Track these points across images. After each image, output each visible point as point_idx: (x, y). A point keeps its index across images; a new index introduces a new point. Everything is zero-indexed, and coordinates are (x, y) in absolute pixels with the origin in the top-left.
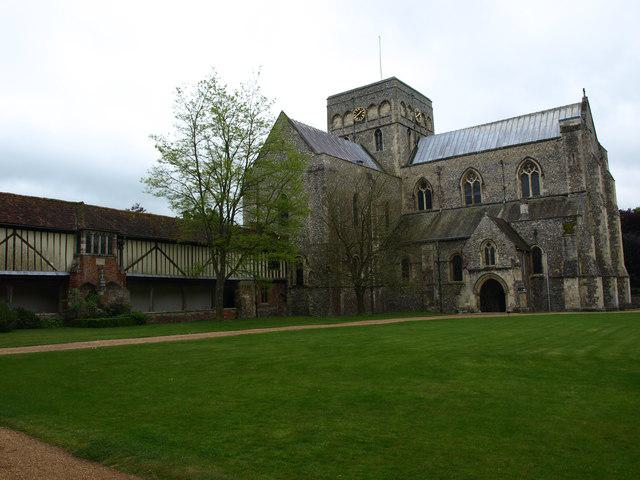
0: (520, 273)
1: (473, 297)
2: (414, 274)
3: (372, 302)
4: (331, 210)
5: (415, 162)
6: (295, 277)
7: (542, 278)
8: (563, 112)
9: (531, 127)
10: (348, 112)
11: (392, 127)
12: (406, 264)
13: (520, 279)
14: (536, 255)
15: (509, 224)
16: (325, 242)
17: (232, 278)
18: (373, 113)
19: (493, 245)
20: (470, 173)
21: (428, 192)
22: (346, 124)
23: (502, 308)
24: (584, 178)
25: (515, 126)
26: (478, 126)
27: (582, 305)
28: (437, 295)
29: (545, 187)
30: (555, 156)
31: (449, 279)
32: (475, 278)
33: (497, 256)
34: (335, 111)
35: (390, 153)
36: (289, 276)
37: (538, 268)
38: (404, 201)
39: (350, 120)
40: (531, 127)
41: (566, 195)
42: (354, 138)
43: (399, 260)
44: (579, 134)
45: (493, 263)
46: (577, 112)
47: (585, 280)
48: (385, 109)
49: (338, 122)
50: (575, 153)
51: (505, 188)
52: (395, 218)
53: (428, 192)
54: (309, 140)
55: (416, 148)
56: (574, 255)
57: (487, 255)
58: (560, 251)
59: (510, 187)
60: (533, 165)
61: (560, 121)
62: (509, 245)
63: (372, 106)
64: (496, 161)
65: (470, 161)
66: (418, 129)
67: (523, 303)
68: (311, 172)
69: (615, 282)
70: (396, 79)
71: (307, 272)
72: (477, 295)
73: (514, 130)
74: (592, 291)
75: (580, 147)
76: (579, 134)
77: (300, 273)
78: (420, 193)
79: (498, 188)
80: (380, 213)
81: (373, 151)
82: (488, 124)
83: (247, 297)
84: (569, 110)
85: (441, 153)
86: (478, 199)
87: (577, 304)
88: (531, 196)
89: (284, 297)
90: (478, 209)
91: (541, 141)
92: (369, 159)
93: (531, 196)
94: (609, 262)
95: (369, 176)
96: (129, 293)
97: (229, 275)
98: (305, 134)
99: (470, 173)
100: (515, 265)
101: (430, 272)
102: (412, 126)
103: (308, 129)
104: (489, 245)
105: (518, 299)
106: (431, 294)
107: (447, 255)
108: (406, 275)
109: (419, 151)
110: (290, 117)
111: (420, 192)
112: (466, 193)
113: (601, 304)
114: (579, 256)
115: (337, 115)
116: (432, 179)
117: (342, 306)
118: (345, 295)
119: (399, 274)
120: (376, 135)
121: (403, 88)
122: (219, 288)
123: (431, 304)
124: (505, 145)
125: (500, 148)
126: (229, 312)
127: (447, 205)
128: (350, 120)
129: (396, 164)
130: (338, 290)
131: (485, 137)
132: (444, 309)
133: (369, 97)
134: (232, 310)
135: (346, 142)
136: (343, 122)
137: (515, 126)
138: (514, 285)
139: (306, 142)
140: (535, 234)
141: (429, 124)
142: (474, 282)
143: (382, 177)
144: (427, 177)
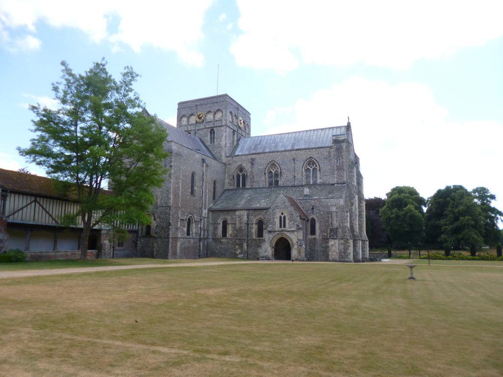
10: (192, 115)
11: (222, 128)
17: (96, 227)
18: (210, 117)
20: (273, 164)
21: (244, 175)
23: (288, 257)
24: (345, 174)
29: (320, 178)
32: (271, 236)
34: (183, 113)
35: (219, 146)
36: (140, 228)
37: (313, 232)
39: (193, 120)
43: (220, 221)
44: (344, 145)
45: (284, 227)
46: (343, 131)
47: (342, 241)
48: (219, 115)
51: (295, 177)
53: (244, 175)
55: (238, 144)
56: (336, 224)
58: (328, 221)
59: (298, 176)
60: (314, 163)
61: (333, 136)
63: (209, 112)
66: (240, 131)
72: (273, 248)
75: (344, 154)
76: (344, 145)
78: (238, 176)
81: (208, 144)
86: (277, 182)
94: (357, 230)
97: (94, 225)
99: (273, 164)
100: (299, 229)
102: (236, 129)
109: (240, 146)
113: (351, 257)
115: (184, 116)
116: (247, 166)
117: (178, 251)
118: (181, 244)
120: (211, 133)
121: (232, 102)
122: (86, 235)
125: (294, 150)
126: (92, 253)
128: (193, 120)
132: (249, 256)
134: (94, 252)
136: (188, 121)
140: (313, 209)
142: (271, 239)
144: (244, 165)
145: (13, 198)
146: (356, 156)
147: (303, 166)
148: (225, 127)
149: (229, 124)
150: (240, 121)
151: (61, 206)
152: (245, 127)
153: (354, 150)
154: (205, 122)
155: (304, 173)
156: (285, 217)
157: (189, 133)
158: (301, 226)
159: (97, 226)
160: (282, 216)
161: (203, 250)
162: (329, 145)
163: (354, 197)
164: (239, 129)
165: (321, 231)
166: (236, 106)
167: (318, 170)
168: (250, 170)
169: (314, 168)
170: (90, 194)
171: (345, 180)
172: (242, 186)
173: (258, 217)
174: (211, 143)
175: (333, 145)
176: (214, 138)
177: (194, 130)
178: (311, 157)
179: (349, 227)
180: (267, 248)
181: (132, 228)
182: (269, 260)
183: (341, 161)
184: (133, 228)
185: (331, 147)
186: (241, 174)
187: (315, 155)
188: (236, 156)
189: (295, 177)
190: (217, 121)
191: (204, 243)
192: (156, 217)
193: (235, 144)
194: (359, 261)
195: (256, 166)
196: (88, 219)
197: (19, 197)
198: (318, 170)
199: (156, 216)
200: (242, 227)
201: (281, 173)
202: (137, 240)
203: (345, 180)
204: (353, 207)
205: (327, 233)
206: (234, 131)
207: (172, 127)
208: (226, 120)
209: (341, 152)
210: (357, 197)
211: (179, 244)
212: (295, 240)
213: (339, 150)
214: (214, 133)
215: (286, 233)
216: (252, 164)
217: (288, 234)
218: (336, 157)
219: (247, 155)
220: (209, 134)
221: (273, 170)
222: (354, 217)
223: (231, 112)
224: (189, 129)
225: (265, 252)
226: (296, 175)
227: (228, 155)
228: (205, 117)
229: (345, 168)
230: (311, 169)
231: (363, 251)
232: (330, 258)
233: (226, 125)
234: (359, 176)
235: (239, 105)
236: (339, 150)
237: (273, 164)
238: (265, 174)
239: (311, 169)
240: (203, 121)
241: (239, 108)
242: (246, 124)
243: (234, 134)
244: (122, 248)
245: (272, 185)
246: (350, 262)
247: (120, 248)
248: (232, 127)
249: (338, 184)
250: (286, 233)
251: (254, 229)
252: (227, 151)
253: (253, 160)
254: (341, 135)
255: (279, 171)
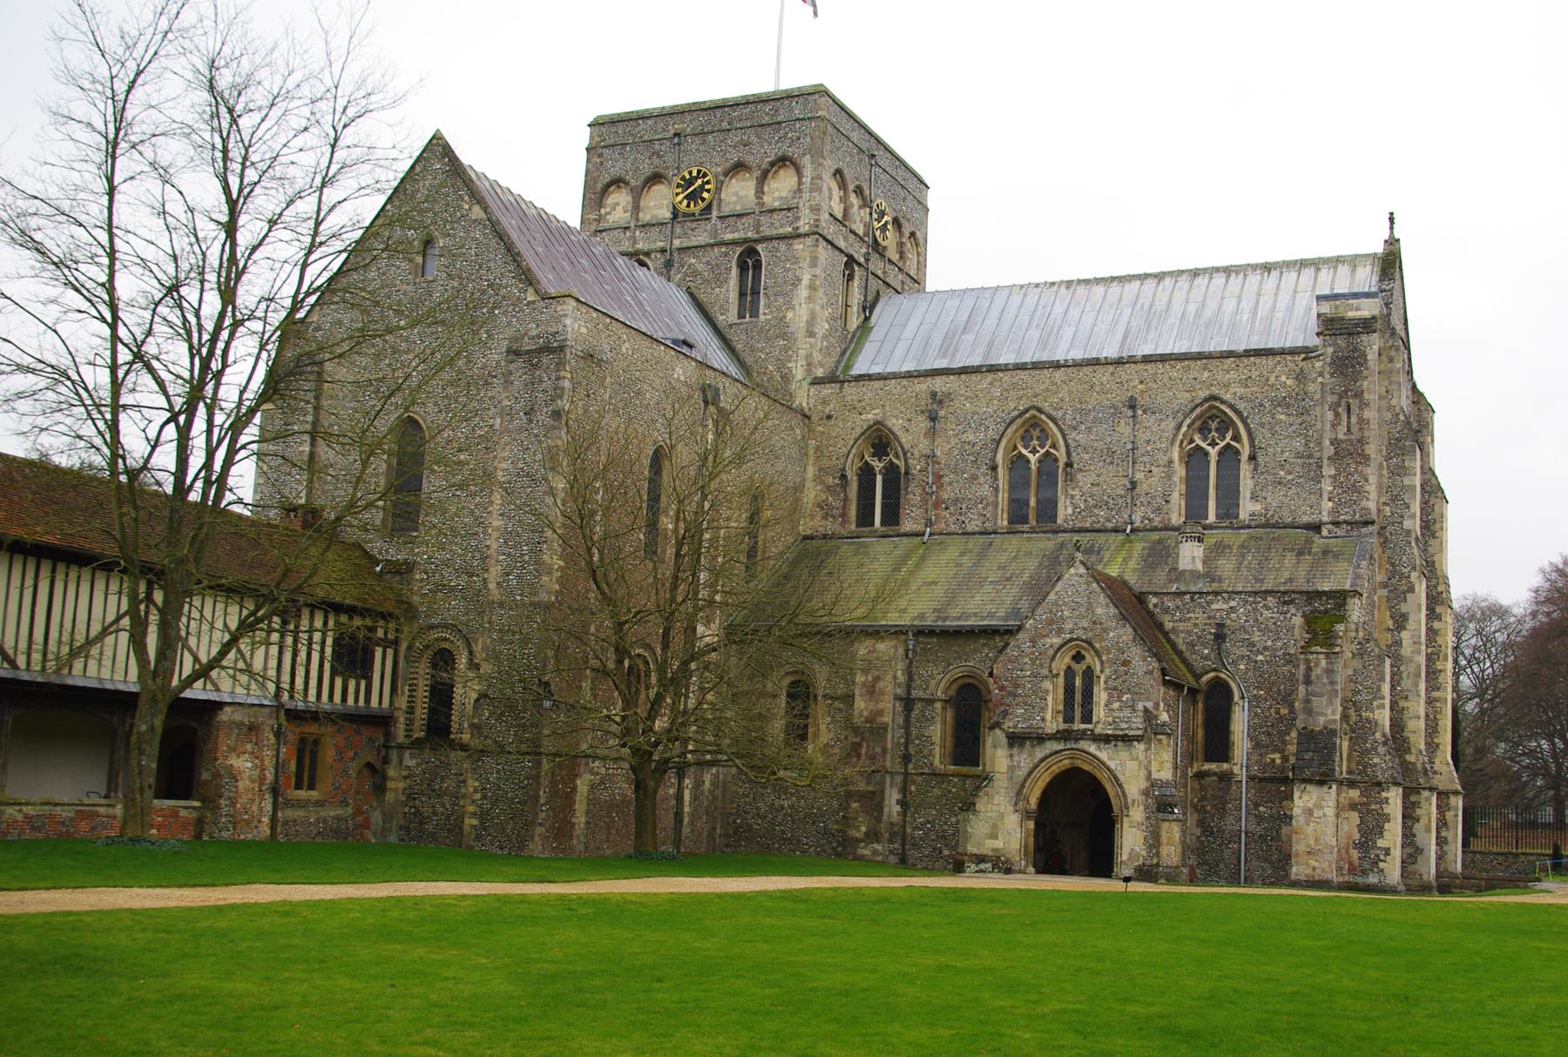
0: (1167, 756)
1: (1012, 821)
2: (824, 729)
3: (678, 816)
4: (579, 491)
5: (860, 368)
6: (421, 712)
7: (1226, 778)
8: (1325, 275)
9: (1230, 306)
10: (656, 178)
11: (798, 246)
12: (801, 693)
13: (1166, 774)
14: (1216, 703)
15: (1141, 598)
16: (544, 597)
17: (197, 692)
18: (739, 192)
19: (1090, 658)
20: (1032, 425)
21: (892, 471)
22: (645, 217)
23: (1101, 862)
24: (1373, 479)
25: (1180, 295)
26: (1069, 283)
27: (1340, 869)
28: (892, 808)
29: (1254, 497)
30: (1295, 403)
31: (938, 759)
32: (1025, 759)
33: (1101, 696)
34: (615, 169)
35: (782, 330)
36: (402, 702)
37: (1217, 744)
38: (811, 495)
39: (659, 202)
40: (1230, 306)
41: (1316, 528)
42: (669, 265)
43: (779, 683)
44: (1373, 344)
45: (1087, 718)
46: (1366, 278)
47: (1354, 794)
48: (781, 186)
49: (618, 205)
50: (1354, 403)
51: (1134, 485)
52: (777, 543)
53: (892, 471)
54: (521, 246)
55: (865, 327)
56: (1329, 713)
57: (1069, 689)
58: (1287, 698)
59: (1150, 484)
60: (1225, 425)
61: (1319, 298)
62: (1142, 664)
63: (739, 167)
64: (1120, 397)
65: (1205, 379)
66: (877, 266)
67: (1171, 853)
68: (517, 353)
69: (1429, 807)
70: (827, 93)
71: (465, 694)
72: (1027, 815)
73: (1177, 308)
74: (1372, 826)
75: (1372, 387)
76: (1373, 344)
77: (442, 696)
78: (866, 474)
79: (1114, 484)
80: (734, 519)
81: (728, 315)
82: (1098, 281)
83: (243, 764)
84: (1344, 270)
85: (1043, 344)
86: (1048, 511)
87: (1325, 867)
88: (1212, 518)
89: (376, 774)
90: (1047, 543)
91: (1259, 353)
92: (715, 343)
93: (1212, 518)
94: (1418, 741)
95: (709, 396)
96: (1129, 630)
97: (188, 683)
98: (510, 224)
99: (1032, 425)
100: (1153, 730)
101: (879, 731)
102: (859, 252)
103: (519, 207)
104: (1078, 657)
105: (1154, 840)
106: (874, 802)
107: (938, 681)
108: (799, 733)
109: (876, 335)
110: (465, 156)
111: (1018, 463)
112: (1013, 487)
113: (1393, 871)
114: (1345, 717)
115: (618, 182)
116: (910, 433)
117: (580, 819)
118: (593, 787)
119: (777, 727)
120: (743, 267)
121: (846, 126)
122: (149, 724)
123: (872, 836)
124: (1147, 350)
125: (1132, 360)
126: (174, 813)
127: (948, 521)
128: (659, 202)
129: (798, 371)
130: (571, 763)
131: (1089, 318)
132: (912, 854)
133: (734, 138)
134: (186, 808)
135: (641, 272)
136: (636, 208)
137: (1180, 295)
138: (1146, 793)
139: (509, 248)
140: (1220, 637)
141: (911, 256)
142: (1022, 773)
143: (754, 406)
144: (895, 424)
145: (75, 586)
146: (1417, 396)
147: (1175, 436)
148: (809, 241)
149: (830, 230)
150: (882, 214)
151: (29, 582)
152: (901, 245)
153: (1410, 372)
154: (715, 213)
155: (1180, 471)
156: (1089, 675)
157: (643, 264)
158: (1164, 717)
159: (199, 684)
160: (1079, 668)
161: (694, 815)
162: (1300, 343)
163: (1411, 589)
164: (874, 257)
165: (1257, 745)
166: (864, 146)
167: (1245, 456)
168: (923, 446)
169: (1228, 446)
170: (174, 528)
171: (1372, 505)
172: (883, 523)
173: (957, 671)
174: (741, 316)
175: (1316, 341)
176: (755, 293)
177: (663, 251)
178: (1214, 398)
179: (1387, 730)
180: (1002, 816)
181: (361, 703)
182: (1008, 871)
183: (1354, 419)
184: (368, 700)
185: (1306, 352)
186: (878, 465)
187: (1232, 387)
188: (860, 378)
189: (1134, 485)
190: (772, 211)
191: (698, 784)
192: (480, 655)
193: (854, 322)
194: (1425, 889)
195: (949, 428)
196: (161, 654)
197: (54, 571)
198: (1245, 456)
199: (478, 648)
200: (881, 713)
201: (1069, 465)
202: (386, 761)
203: (1372, 505)
204: (1405, 635)
205: (1281, 751)
206: (851, 261)
207: (565, 229)
208: (816, 209)
209: (1356, 376)
210: (1421, 588)
211: (582, 785)
212: (1134, 786)
213: (1348, 366)
214: (758, 266)
215: (1092, 748)
216: (933, 419)
217: (1103, 755)
218: (1330, 399)
219: (909, 375)
220: (734, 272)
221: (1034, 451)
222: (1406, 683)
223: (838, 173)
224: (640, 246)
225: (994, 836)
226: (1139, 476)
227: (820, 373)
228: (719, 190)
229: (1371, 450)
230: (1213, 452)
231: (1441, 842)
232: (1298, 870)
233: (816, 233)
234: (1433, 491)
235: (879, 141)
236: (1348, 366)
237: (1034, 424)
238: (994, 468)
239: (1213, 452)
240: (708, 208)
241: (880, 153)
242: (907, 231)
243: (850, 278)
244: (314, 794)
245: (1025, 520)
246: (1393, 890)
247: (303, 794)
248: (842, 244)
249: (1336, 524)
250: (1092, 748)
251: (937, 731)
252: (817, 357)
253: (937, 399)
254: (1356, 296)
255: (1062, 459)
